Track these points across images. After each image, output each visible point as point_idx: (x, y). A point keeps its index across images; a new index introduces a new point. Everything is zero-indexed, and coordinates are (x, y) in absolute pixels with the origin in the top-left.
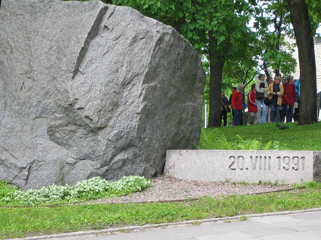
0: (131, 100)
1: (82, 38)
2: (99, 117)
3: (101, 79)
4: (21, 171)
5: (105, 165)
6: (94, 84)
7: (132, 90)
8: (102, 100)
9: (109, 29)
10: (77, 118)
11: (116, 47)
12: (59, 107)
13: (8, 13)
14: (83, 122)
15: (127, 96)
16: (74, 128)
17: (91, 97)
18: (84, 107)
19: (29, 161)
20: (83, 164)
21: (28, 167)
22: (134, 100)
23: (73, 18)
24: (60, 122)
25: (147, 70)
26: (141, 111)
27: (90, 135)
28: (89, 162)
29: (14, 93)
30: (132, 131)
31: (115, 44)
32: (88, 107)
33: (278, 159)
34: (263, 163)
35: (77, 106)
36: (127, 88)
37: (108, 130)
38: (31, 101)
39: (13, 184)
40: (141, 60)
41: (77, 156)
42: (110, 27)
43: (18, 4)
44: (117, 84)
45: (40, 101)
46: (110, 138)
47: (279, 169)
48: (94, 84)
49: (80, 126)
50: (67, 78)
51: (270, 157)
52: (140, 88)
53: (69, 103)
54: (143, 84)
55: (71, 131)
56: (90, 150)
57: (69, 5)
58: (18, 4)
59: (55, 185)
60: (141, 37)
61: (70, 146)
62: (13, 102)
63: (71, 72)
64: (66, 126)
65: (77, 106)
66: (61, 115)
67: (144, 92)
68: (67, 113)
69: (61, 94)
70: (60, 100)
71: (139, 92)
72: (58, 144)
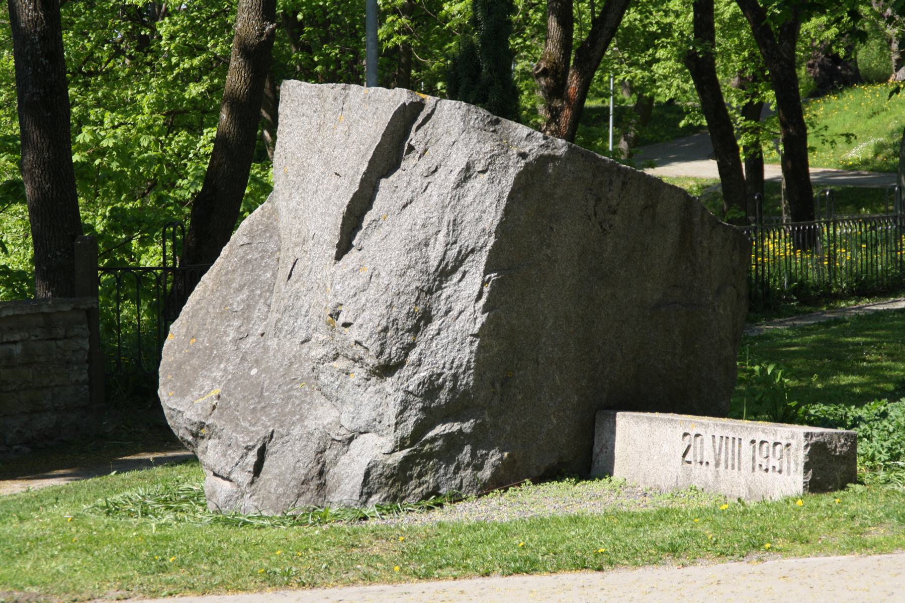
2: (382, 344)
5: (402, 447)
8: (391, 306)
17: (367, 301)
18: (351, 321)
21: (259, 446)
25: (492, 241)
26: (481, 329)
32: (360, 321)
37: (406, 371)
40: (479, 220)
46: (411, 389)
48: (376, 272)
51: (740, 439)
52: (479, 281)
54: (486, 272)
60: (480, 169)
67: (486, 289)
71: (477, 288)
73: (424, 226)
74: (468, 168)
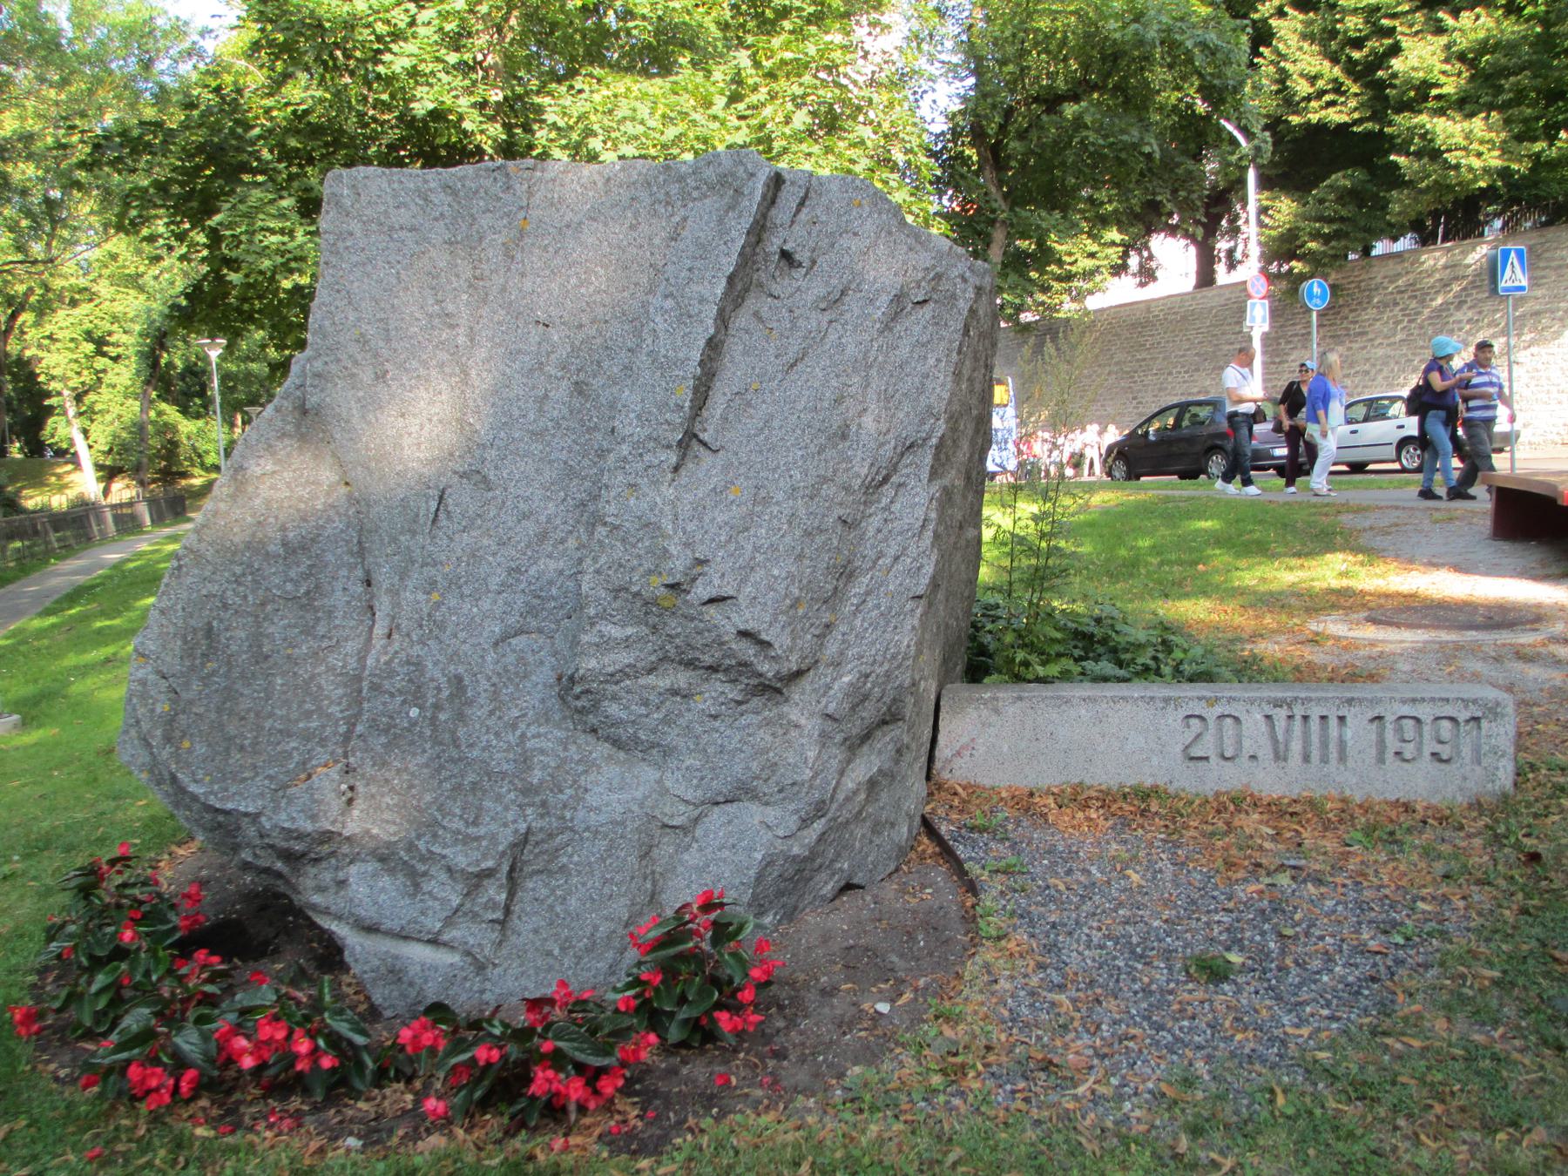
0: (892, 551)
1: (702, 300)
3: (789, 470)
4: (477, 886)
6: (763, 493)
7: (896, 507)
8: (800, 557)
9: (800, 265)
10: (699, 641)
11: (833, 337)
12: (615, 598)
13: (355, 226)
14: (731, 654)
15: (879, 531)
16: (682, 678)
17: (756, 549)
18: (731, 593)
19: (506, 837)
20: (730, 822)
21: (505, 868)
22: (905, 549)
23: (632, 227)
24: (624, 658)
27: (756, 702)
28: (752, 813)
29: (402, 538)
30: (899, 667)
31: (824, 325)
33: (1374, 726)
34: (1315, 738)
35: (701, 591)
36: (879, 501)
37: (824, 674)
38: (483, 570)
39: (445, 944)
40: (921, 390)
41: (699, 793)
42: (802, 256)
43: (396, 186)
44: (847, 489)
45: (517, 570)
47: (1381, 760)
48: (763, 493)
49: (713, 669)
50: (650, 472)
52: (923, 498)
53: (670, 581)
55: (675, 692)
56: (754, 765)
57: (608, 180)
58: (396, 186)
61: (668, 752)
62: (403, 575)
63: (669, 447)
64: (650, 671)
65: (701, 591)
66: (630, 631)
68: (652, 620)
69: (623, 540)
70: (621, 565)
72: (617, 743)
73: (838, 401)
74: (898, 298)
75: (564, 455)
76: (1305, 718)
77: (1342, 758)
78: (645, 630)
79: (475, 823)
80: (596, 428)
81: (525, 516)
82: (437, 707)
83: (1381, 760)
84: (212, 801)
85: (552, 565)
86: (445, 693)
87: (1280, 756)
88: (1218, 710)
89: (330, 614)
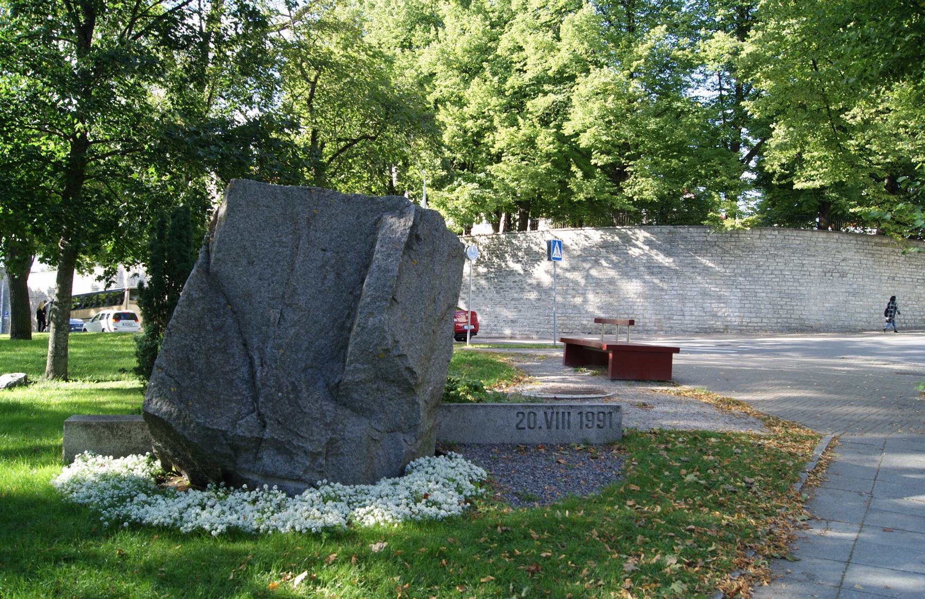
16: (382, 385)
24: (363, 376)
34: (560, 420)
35: (395, 353)
47: (581, 428)
49: (393, 382)
59: (746, 109)
72: (354, 410)
75: (331, 300)
76: (557, 413)
77: (569, 428)
78: (371, 366)
79: (312, 435)
80: (344, 291)
81: (316, 322)
82: (288, 393)
83: (581, 428)
84: (207, 425)
85: (323, 342)
86: (290, 388)
87: (549, 427)
88: (529, 410)
89: (233, 356)
